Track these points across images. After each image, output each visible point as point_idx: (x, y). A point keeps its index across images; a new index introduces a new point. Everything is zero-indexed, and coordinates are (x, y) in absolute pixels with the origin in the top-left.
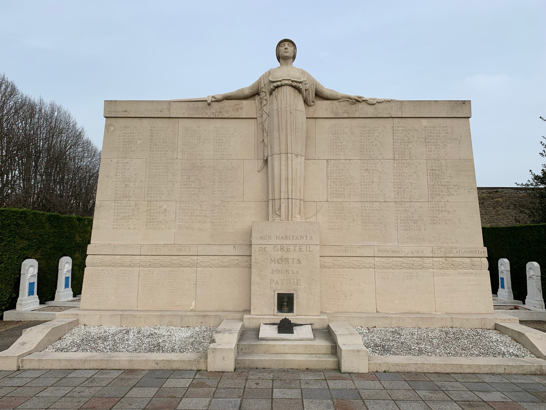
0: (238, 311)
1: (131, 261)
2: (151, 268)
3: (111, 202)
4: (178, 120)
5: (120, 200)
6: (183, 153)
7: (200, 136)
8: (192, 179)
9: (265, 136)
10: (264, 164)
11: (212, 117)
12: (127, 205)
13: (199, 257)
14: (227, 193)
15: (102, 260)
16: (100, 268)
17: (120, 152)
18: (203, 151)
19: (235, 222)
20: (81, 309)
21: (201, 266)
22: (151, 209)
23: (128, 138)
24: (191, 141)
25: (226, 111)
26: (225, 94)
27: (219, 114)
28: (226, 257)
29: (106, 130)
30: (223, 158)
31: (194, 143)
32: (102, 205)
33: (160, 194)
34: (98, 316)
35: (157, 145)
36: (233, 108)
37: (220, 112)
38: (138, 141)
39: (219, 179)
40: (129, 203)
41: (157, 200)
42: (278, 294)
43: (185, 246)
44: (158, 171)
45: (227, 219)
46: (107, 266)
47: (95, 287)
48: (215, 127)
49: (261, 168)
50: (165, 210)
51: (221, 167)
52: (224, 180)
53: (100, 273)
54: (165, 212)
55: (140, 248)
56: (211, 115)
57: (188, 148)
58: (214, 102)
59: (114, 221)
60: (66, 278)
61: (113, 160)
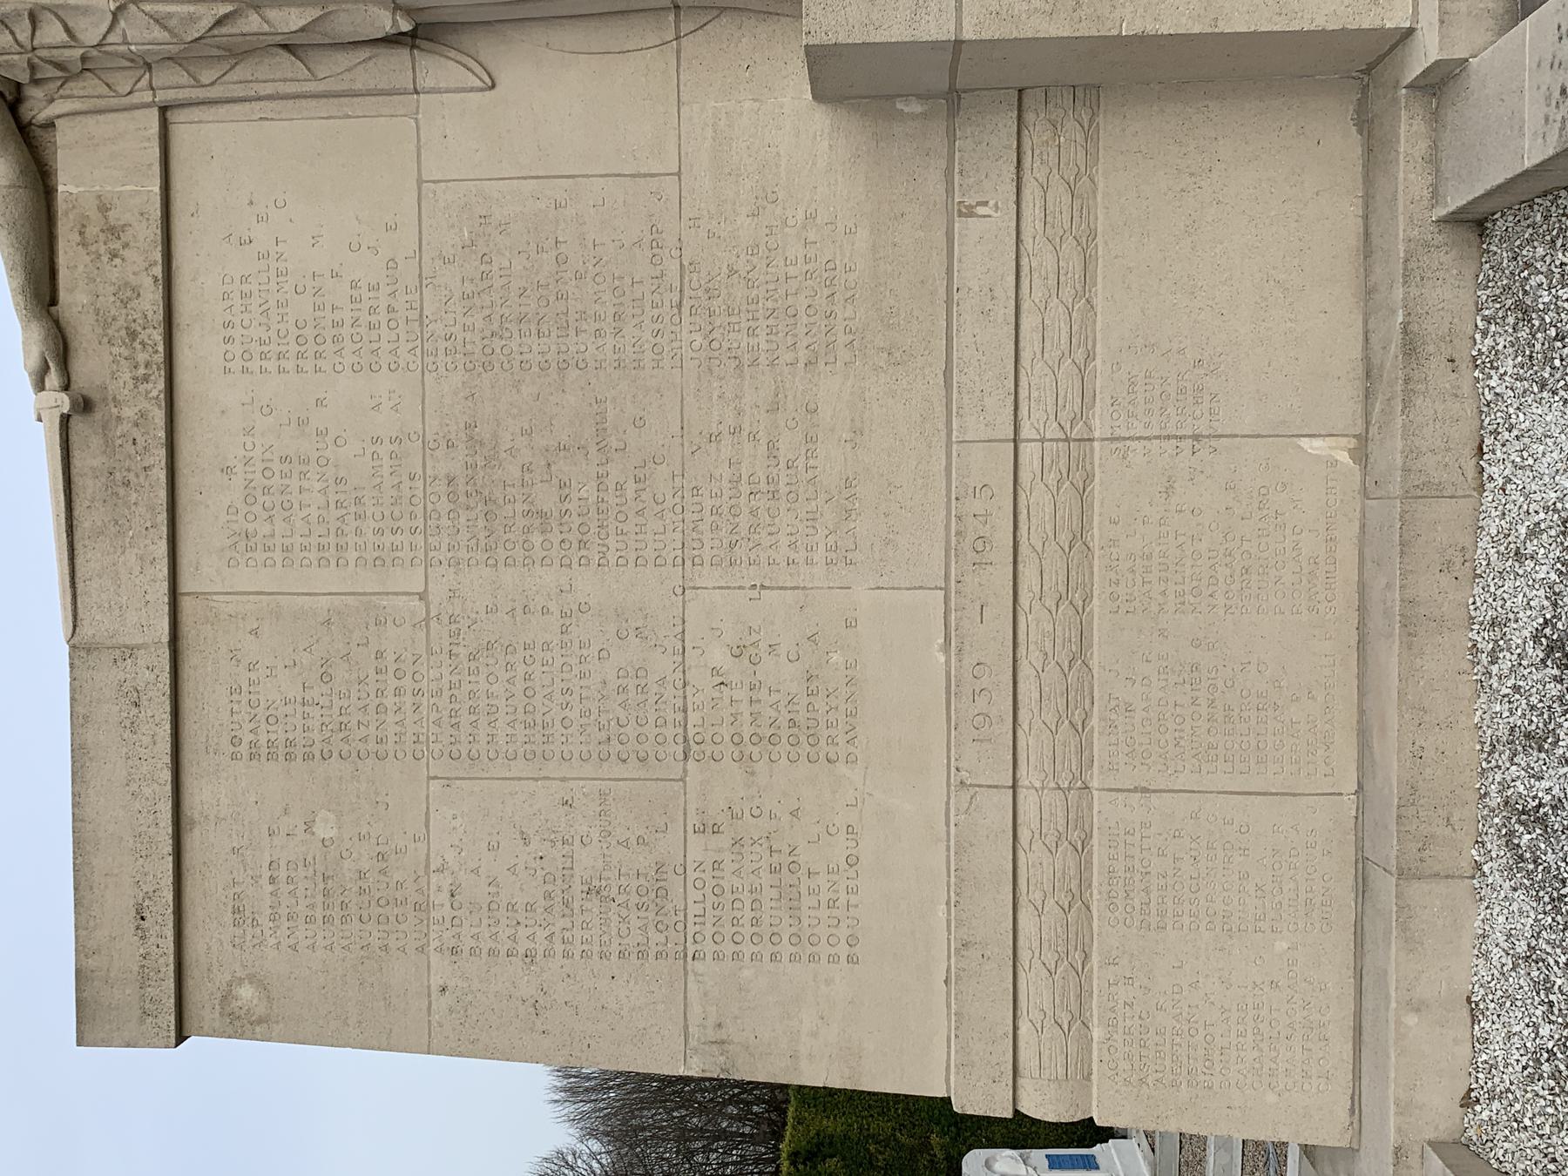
0: (1368, 179)
1: (1051, 840)
2: (1094, 721)
3: (691, 978)
4: (188, 594)
5: (680, 927)
6: (388, 562)
7: (284, 459)
8: (547, 499)
9: (266, 28)
10: (453, 54)
11: (161, 385)
12: (710, 883)
13: (1026, 432)
14: (628, 281)
15: (1049, 1022)
16: (1097, 1033)
17: (393, 944)
18: (376, 440)
19: (810, 217)
20: (1348, 1136)
21: (1082, 416)
22: (736, 739)
23: (300, 892)
24: (315, 513)
25: (125, 304)
26: (17, 304)
27: (143, 344)
28: (1024, 261)
29: (258, 1029)
30: (414, 315)
31: (324, 491)
32: (712, 1035)
33: (643, 689)
34: (1411, 1020)
35: (344, 719)
36: (105, 259)
38: (322, 831)
39: (544, 329)
40: (697, 875)
41: (679, 703)
43: (959, 518)
44: (501, 703)
45: (792, 271)
46: (1083, 995)
47: (1216, 1057)
48: (227, 371)
50: (738, 652)
51: (469, 321)
52: (552, 299)
53: (1127, 1032)
54: (752, 651)
55: (972, 791)
56: (147, 392)
57: (358, 532)
58: (74, 378)
59: (805, 958)
60: (1051, 1167)
61: (436, 982)
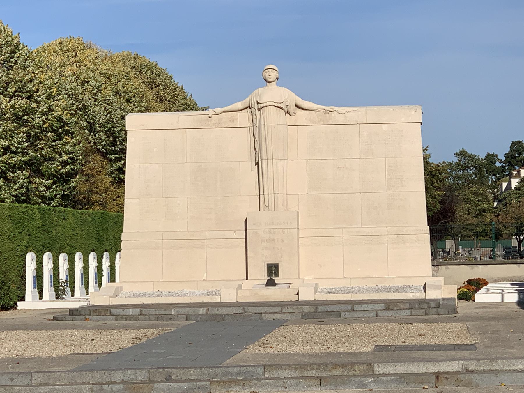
37: (219, 123)
42: (267, 264)
49: (268, 289)
